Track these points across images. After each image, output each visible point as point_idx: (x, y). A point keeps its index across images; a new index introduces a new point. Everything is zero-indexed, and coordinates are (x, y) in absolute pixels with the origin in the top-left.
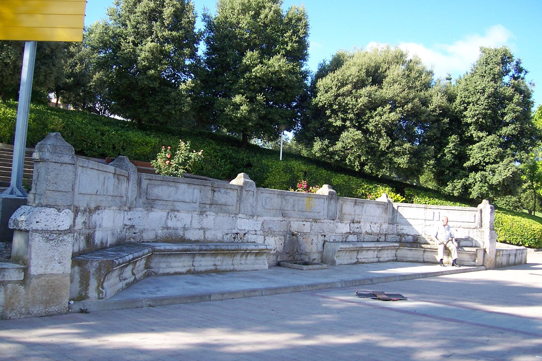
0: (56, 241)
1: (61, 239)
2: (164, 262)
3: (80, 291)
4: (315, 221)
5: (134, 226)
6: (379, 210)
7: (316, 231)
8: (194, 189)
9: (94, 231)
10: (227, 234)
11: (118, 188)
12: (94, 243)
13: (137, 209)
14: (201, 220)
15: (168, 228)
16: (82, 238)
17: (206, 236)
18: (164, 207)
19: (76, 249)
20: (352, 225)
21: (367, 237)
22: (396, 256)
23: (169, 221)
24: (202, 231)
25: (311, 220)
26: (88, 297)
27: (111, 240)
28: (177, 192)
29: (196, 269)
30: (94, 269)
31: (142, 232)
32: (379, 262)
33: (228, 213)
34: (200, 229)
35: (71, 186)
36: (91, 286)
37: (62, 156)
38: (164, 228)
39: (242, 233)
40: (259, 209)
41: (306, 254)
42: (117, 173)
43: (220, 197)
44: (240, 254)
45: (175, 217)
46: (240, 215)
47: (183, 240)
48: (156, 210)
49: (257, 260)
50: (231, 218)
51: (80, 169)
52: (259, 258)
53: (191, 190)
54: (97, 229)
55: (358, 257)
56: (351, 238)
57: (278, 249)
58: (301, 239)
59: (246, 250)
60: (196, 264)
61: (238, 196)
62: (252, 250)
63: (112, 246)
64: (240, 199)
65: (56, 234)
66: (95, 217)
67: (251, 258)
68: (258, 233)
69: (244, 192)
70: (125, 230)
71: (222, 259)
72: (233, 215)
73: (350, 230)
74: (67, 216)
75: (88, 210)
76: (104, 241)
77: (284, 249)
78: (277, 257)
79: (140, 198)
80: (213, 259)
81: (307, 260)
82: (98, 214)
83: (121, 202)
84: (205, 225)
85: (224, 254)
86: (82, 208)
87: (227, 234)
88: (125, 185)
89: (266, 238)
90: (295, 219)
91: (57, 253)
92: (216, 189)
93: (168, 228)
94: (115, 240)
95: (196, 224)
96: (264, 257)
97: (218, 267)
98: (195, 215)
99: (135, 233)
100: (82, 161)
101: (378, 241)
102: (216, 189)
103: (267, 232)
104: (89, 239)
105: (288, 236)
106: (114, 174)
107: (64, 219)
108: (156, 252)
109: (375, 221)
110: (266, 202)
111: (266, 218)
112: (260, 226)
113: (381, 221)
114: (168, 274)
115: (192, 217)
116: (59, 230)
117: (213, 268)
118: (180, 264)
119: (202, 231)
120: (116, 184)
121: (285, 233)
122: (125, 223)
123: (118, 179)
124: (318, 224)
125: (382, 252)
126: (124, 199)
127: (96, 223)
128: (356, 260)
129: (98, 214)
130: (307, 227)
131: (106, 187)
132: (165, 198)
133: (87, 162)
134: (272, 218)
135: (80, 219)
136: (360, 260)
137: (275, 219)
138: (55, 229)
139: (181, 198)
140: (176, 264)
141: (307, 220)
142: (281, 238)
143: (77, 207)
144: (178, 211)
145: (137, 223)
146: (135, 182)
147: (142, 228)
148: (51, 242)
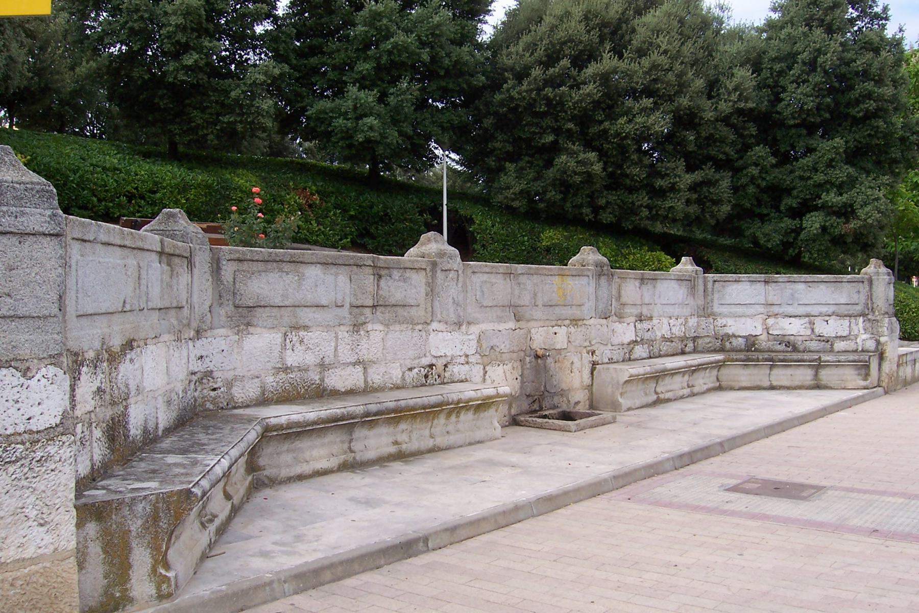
0: (27, 462)
1: (39, 454)
2: (288, 451)
3: (109, 586)
4: (575, 322)
5: (212, 372)
6: (681, 292)
7: (577, 343)
8: (336, 275)
9: (126, 407)
10: (410, 369)
11: (171, 287)
12: (127, 436)
13: (216, 331)
14: (355, 343)
15: (287, 368)
16: (98, 433)
17: (369, 379)
18: (276, 322)
19: (84, 469)
20: (639, 326)
21: (665, 347)
23: (289, 352)
24: (359, 369)
25: (567, 322)
26: (131, 600)
27: (164, 418)
28: (300, 285)
29: (358, 458)
30: (140, 522)
31: (229, 384)
32: (693, 395)
33: (412, 322)
34: (354, 364)
35: (56, 297)
36: (135, 568)
37: (23, 214)
38: (278, 370)
39: (440, 363)
40: (472, 311)
41: (562, 393)
42: (167, 250)
43: (392, 289)
44: (446, 411)
45: (301, 342)
46: (435, 325)
47: (321, 393)
48: (258, 330)
49: (478, 419)
50: (416, 333)
51: (76, 247)
52: (482, 415)
53: (329, 278)
54: (132, 400)
55: (659, 390)
56: (640, 351)
58: (553, 364)
59: (459, 402)
60: (356, 446)
61: (428, 284)
62: (471, 400)
63: (168, 431)
64: (432, 291)
65: (23, 443)
66: (125, 369)
67: (467, 417)
68: (472, 359)
69: (439, 274)
70: (192, 386)
71: (409, 427)
72: (420, 327)
73: (636, 336)
74: (51, 388)
75: (106, 356)
76: (151, 425)
77: (521, 388)
78: (510, 407)
79: (221, 305)
80: (391, 429)
82: (132, 360)
83: (180, 321)
84: (365, 355)
85: (414, 416)
86: (91, 355)
87: (410, 369)
88: (184, 278)
89: (487, 368)
90: (541, 323)
91: (33, 498)
92: (383, 272)
93: (286, 369)
94: (174, 414)
95: (346, 355)
96: (492, 411)
97: (404, 446)
98: (343, 333)
99: (214, 390)
100: (79, 225)
101: (683, 353)
102: (383, 272)
103: (488, 356)
104: (115, 430)
105: (528, 359)
106: (161, 253)
107: (44, 395)
108: (271, 431)
109: (676, 314)
110: (482, 291)
111: (484, 326)
112: (474, 344)
113: (687, 311)
114: (301, 478)
115: (337, 337)
116: (31, 432)
117: (392, 449)
118: (323, 452)
119: (359, 369)
120: (166, 277)
121: (522, 354)
122: (191, 368)
123: (169, 265)
124: (579, 329)
125: (696, 375)
126: (186, 311)
127: (127, 386)
128: (655, 397)
129: (132, 360)
130: (561, 337)
131: (143, 288)
132: (277, 301)
133: (94, 228)
134: (497, 327)
135: (88, 384)
136: (662, 396)
137: (503, 326)
138: (21, 429)
139: (310, 298)
140: (315, 453)
141: (559, 322)
143: (77, 354)
144: (306, 328)
145: (219, 365)
146: (207, 267)
147: (230, 375)
148: (11, 469)
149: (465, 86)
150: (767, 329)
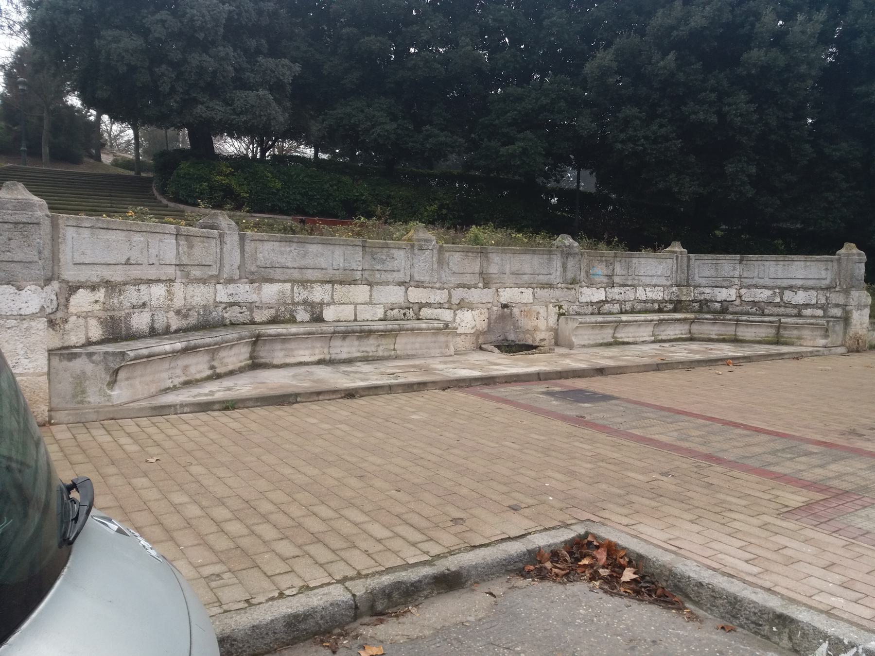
1: (25, 326)
2: (281, 350)
22: (690, 333)
55: (617, 335)
57: (479, 327)
81: (530, 342)
116: (21, 315)
125: (662, 328)
140: (301, 352)
142: (483, 311)
149: (250, 155)
150: (740, 297)
